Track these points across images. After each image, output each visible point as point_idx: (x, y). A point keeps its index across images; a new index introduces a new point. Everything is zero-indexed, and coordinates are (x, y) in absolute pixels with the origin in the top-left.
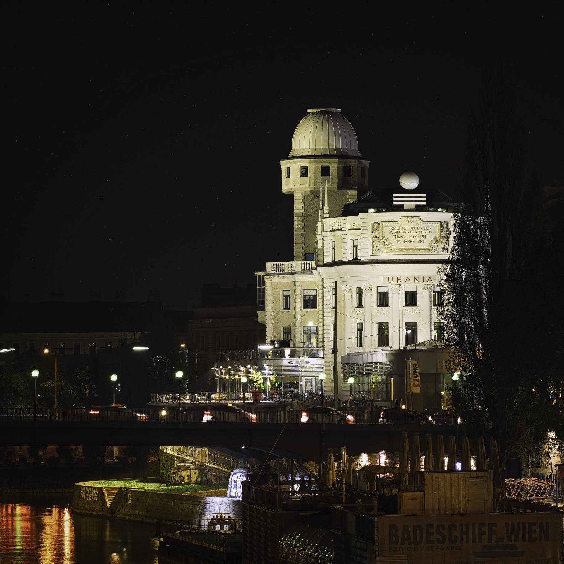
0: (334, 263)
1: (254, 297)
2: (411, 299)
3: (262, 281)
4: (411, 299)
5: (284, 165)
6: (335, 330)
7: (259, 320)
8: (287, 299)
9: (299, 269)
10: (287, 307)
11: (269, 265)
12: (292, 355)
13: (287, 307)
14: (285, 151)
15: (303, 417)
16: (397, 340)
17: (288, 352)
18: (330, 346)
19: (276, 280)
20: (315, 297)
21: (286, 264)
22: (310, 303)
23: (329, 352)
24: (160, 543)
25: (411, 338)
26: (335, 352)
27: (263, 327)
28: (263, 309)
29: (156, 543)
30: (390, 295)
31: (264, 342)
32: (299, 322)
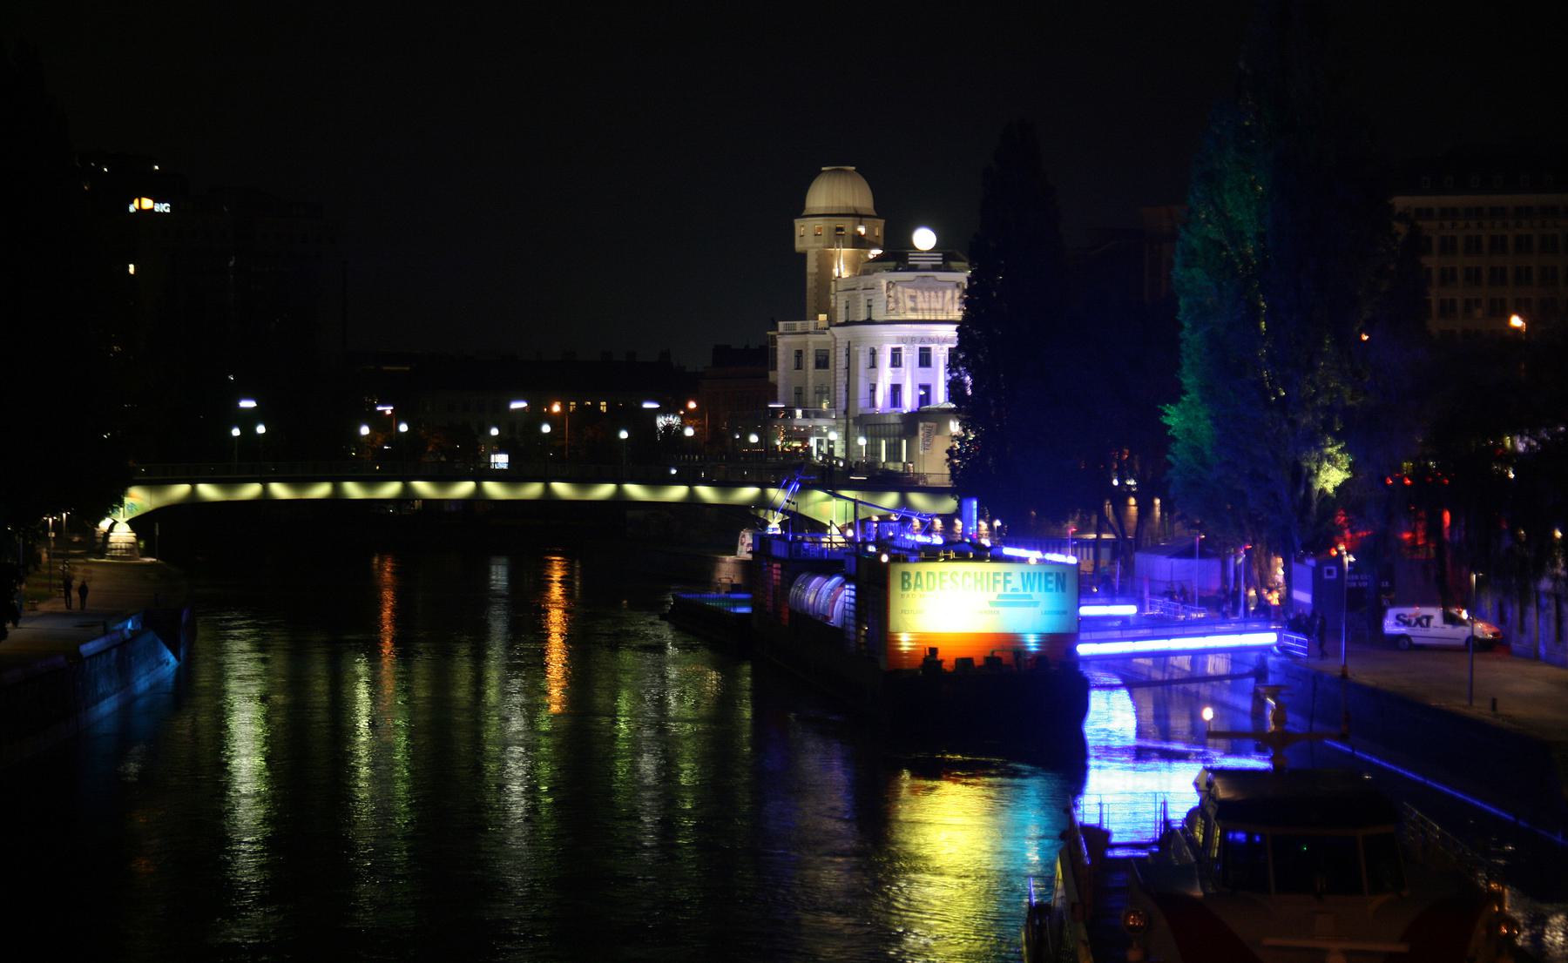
0: (847, 323)
1: (765, 356)
2: (925, 359)
3: (774, 341)
4: (925, 359)
5: (798, 223)
6: (847, 391)
7: (771, 379)
8: (799, 354)
9: (811, 329)
10: (799, 366)
11: (781, 325)
12: (805, 415)
13: (799, 366)
14: (799, 210)
15: (236, 658)
16: (909, 402)
17: (799, 412)
18: (842, 405)
19: (789, 339)
20: (827, 358)
21: (798, 323)
22: (823, 362)
23: (841, 413)
24: (664, 411)
25: (925, 399)
26: (846, 412)
27: (774, 387)
28: (775, 368)
29: (668, 428)
30: (903, 352)
31: (776, 401)
32: (811, 382)
